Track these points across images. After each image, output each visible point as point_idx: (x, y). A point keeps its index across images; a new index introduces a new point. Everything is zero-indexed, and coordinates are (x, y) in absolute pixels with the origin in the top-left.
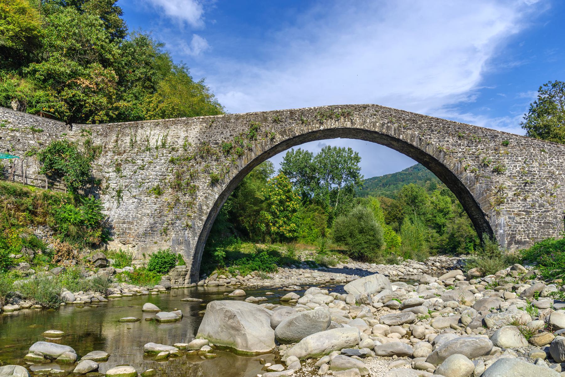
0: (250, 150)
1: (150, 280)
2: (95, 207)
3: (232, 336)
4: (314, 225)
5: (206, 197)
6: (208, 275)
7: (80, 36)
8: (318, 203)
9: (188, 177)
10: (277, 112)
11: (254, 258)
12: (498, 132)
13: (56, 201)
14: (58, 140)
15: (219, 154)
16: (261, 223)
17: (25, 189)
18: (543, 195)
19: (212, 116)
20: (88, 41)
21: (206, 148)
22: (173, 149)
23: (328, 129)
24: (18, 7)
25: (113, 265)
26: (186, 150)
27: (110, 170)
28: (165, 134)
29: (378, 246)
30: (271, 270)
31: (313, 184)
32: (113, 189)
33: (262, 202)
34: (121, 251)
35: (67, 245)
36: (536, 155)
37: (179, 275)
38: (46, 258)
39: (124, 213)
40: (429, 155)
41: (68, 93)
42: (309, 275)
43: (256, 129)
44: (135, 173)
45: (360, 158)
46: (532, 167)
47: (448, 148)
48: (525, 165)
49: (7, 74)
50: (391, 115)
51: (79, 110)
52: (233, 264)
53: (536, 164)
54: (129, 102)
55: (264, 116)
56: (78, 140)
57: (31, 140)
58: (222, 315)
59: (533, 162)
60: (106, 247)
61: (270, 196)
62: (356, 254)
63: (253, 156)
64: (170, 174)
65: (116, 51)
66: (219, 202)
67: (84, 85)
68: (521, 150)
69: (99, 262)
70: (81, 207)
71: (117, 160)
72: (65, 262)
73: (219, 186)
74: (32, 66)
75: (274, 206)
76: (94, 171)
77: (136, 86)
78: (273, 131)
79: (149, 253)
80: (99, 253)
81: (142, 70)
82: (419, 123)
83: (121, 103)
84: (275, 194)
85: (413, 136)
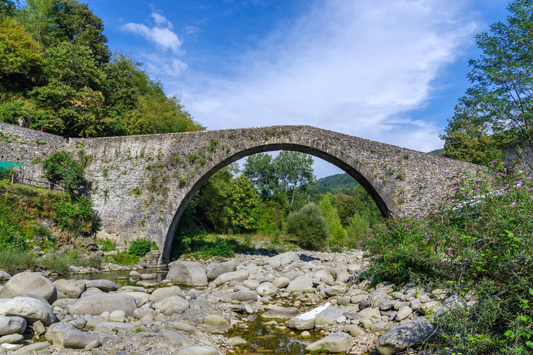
0: (211, 160)
1: (130, 261)
2: (87, 204)
3: (184, 278)
4: (271, 219)
5: (175, 197)
6: (177, 259)
10: (232, 130)
11: (215, 246)
12: (401, 148)
13: (58, 199)
14: (57, 150)
15: (186, 163)
17: (35, 190)
18: (433, 197)
19: (180, 133)
20: (80, 68)
21: (176, 158)
22: (149, 159)
23: (271, 144)
25: (101, 249)
26: (159, 159)
27: (99, 174)
28: (143, 147)
29: (324, 237)
30: (229, 255)
31: (272, 183)
32: (101, 190)
33: (225, 199)
34: (107, 238)
38: (51, 243)
40: (349, 166)
42: (260, 259)
43: (215, 144)
44: (119, 177)
45: (313, 161)
46: (426, 175)
47: (363, 160)
48: (420, 174)
49: (14, 95)
50: (320, 134)
51: (72, 124)
52: (197, 251)
53: (428, 173)
54: (113, 118)
55: (221, 134)
56: (74, 151)
57: (36, 150)
58: (179, 267)
60: (95, 235)
61: (232, 194)
62: (305, 244)
63: (213, 165)
65: (103, 76)
66: (185, 201)
67: (77, 105)
68: (418, 162)
69: (91, 247)
70: (77, 204)
71: (104, 167)
73: (185, 188)
74: (35, 90)
75: (235, 203)
76: (86, 175)
79: (129, 240)
80: (90, 240)
82: (342, 140)
83: (107, 120)
85: (336, 151)
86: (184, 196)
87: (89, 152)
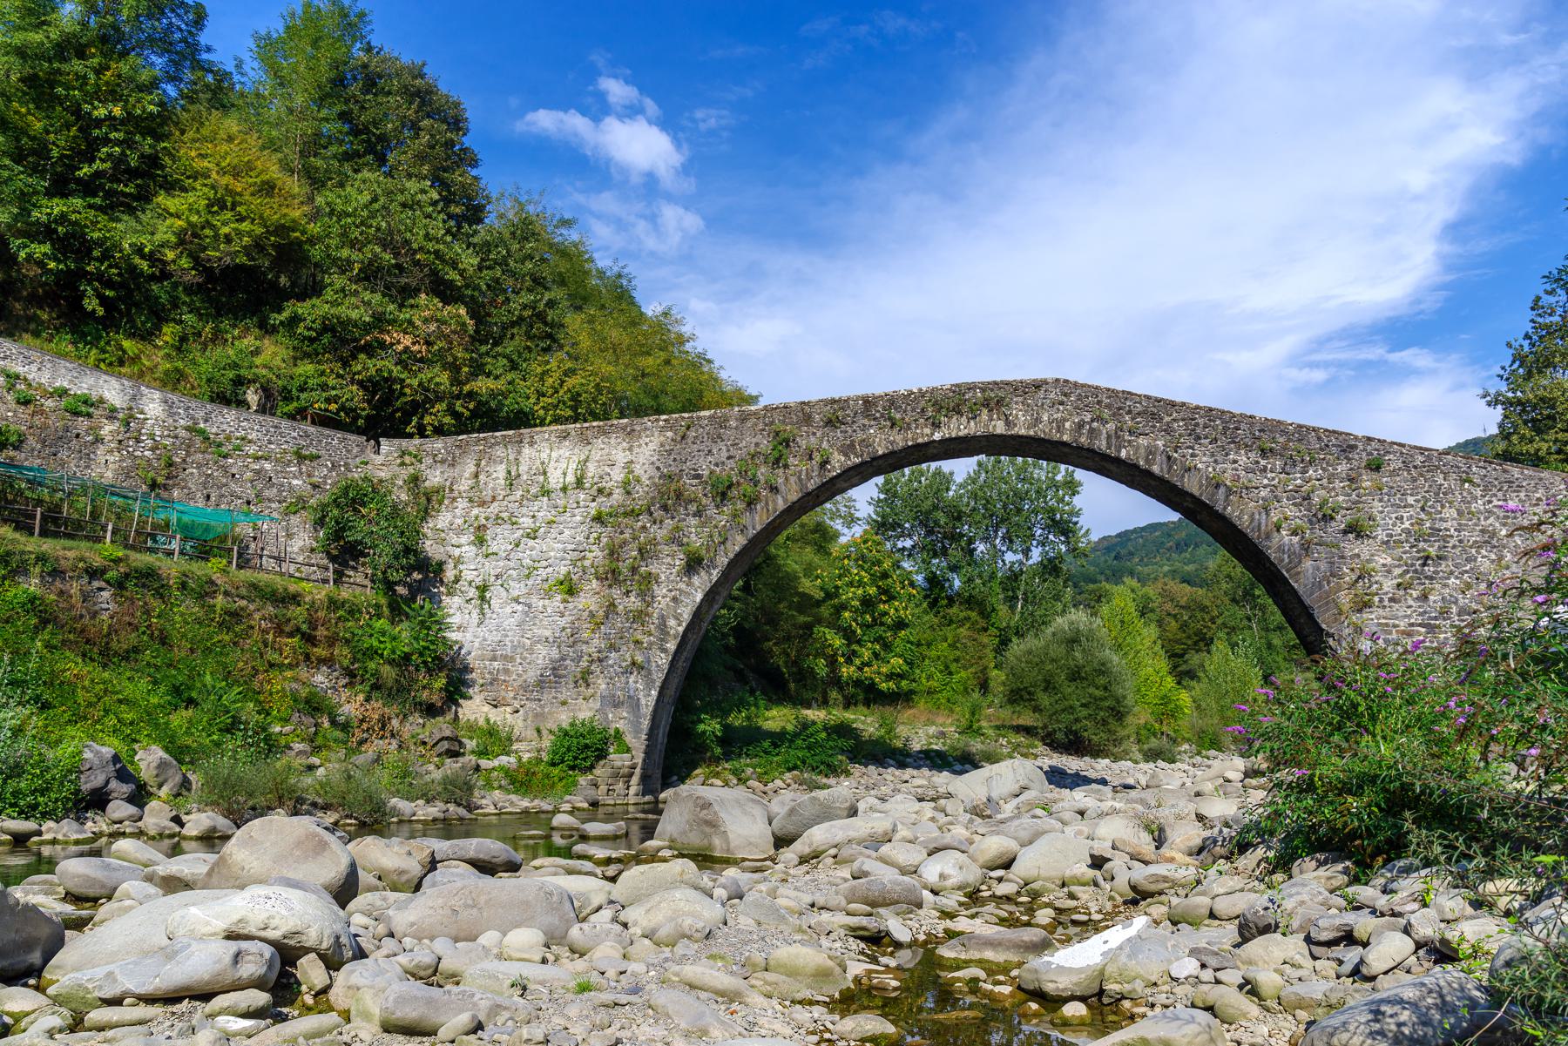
0: (774, 489)
1: (553, 786)
2: (432, 624)
4: (957, 660)
5: (674, 599)
6: (682, 780)
7: (391, 233)
8: (970, 601)
9: (634, 553)
10: (834, 401)
12: (1356, 438)
13: (353, 612)
15: (704, 501)
16: (816, 657)
18: (1469, 586)
22: (600, 491)
23: (951, 439)
24: (258, 180)
25: (473, 752)
26: (628, 493)
27: (464, 540)
28: (583, 457)
29: (1119, 714)
30: (833, 770)
31: (955, 554)
33: (818, 603)
34: (488, 720)
35: (377, 708)
36: (1450, 491)
37: (616, 776)
38: (338, 734)
39: (494, 637)
41: (367, 366)
42: (925, 782)
43: (786, 442)
46: (1441, 519)
47: (1237, 479)
48: (1423, 516)
49: (234, 326)
50: (1099, 403)
51: (388, 400)
52: (740, 756)
53: (1449, 513)
54: (497, 378)
55: (804, 413)
56: (395, 477)
57: (295, 477)
58: (690, 804)
59: (1443, 506)
61: (837, 587)
62: (1060, 736)
63: (781, 505)
64: (594, 548)
65: (470, 261)
67: (400, 348)
68: (1414, 480)
69: (445, 745)
70: (405, 625)
72: (376, 745)
73: (703, 573)
75: (847, 614)
76: (428, 543)
77: (513, 336)
78: (825, 445)
80: (440, 726)
81: (527, 298)
82: (1167, 419)
83: (482, 385)
84: (851, 584)
85: (1151, 451)
86: (699, 597)
87: (434, 477)
